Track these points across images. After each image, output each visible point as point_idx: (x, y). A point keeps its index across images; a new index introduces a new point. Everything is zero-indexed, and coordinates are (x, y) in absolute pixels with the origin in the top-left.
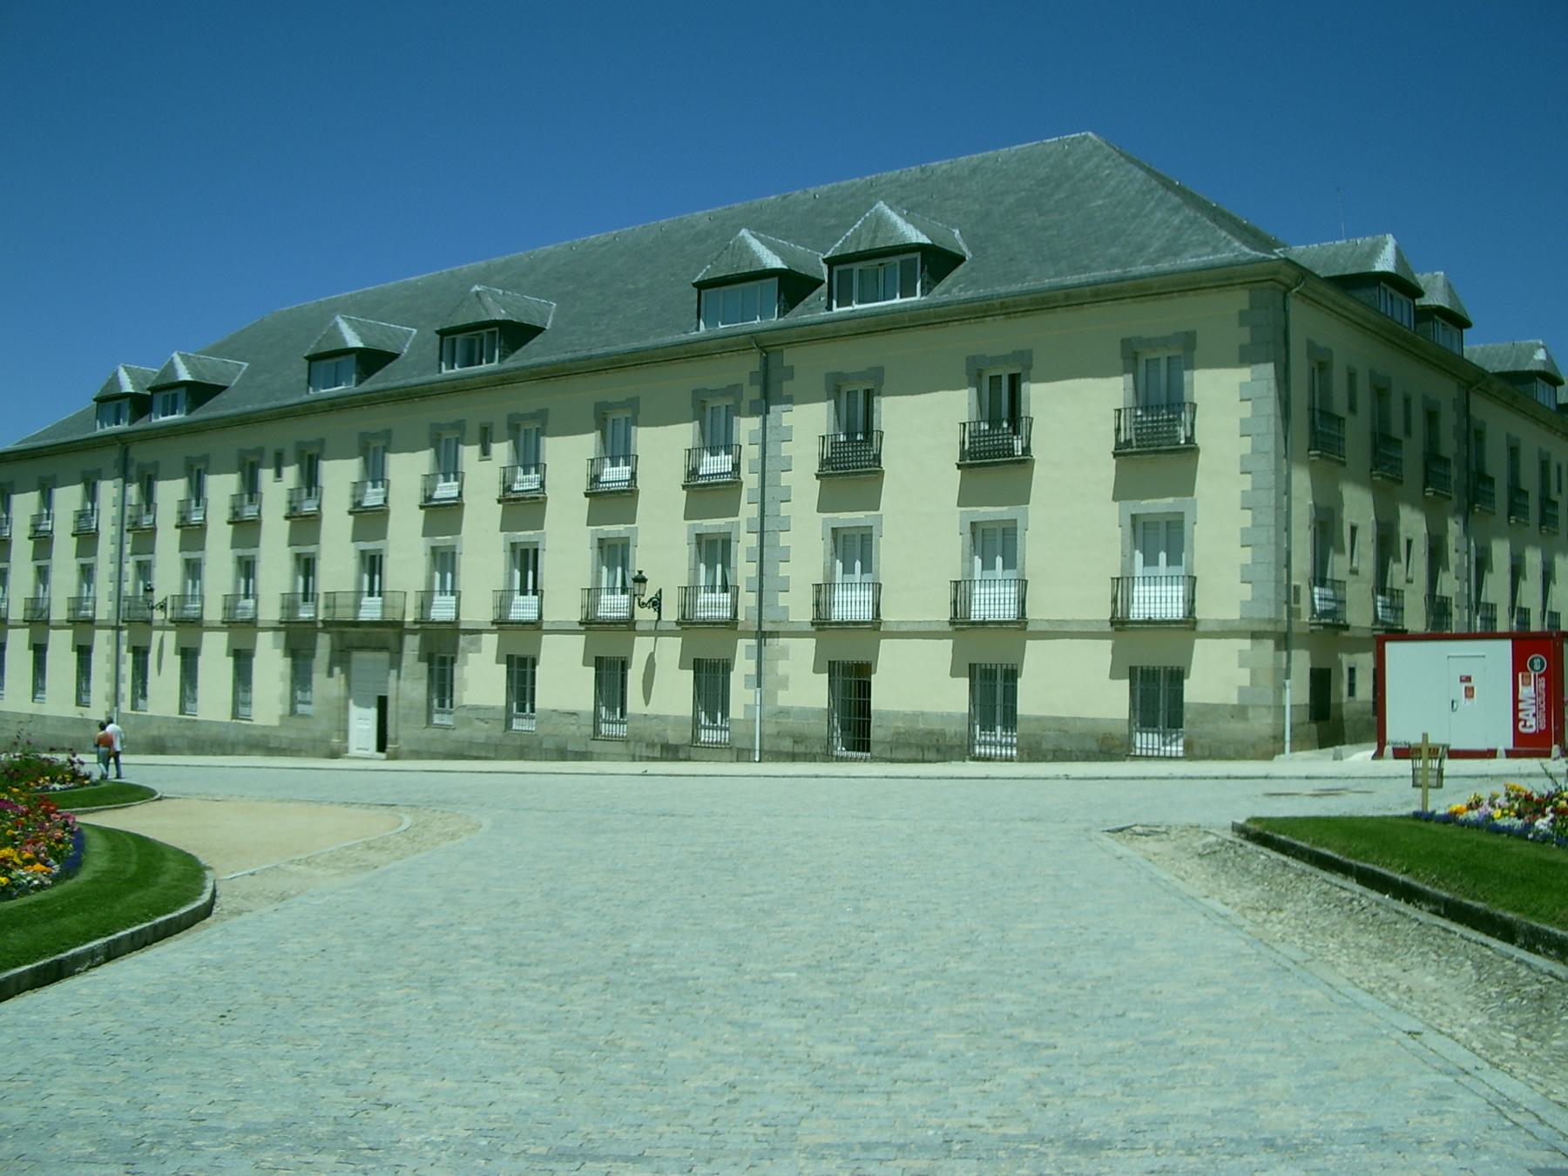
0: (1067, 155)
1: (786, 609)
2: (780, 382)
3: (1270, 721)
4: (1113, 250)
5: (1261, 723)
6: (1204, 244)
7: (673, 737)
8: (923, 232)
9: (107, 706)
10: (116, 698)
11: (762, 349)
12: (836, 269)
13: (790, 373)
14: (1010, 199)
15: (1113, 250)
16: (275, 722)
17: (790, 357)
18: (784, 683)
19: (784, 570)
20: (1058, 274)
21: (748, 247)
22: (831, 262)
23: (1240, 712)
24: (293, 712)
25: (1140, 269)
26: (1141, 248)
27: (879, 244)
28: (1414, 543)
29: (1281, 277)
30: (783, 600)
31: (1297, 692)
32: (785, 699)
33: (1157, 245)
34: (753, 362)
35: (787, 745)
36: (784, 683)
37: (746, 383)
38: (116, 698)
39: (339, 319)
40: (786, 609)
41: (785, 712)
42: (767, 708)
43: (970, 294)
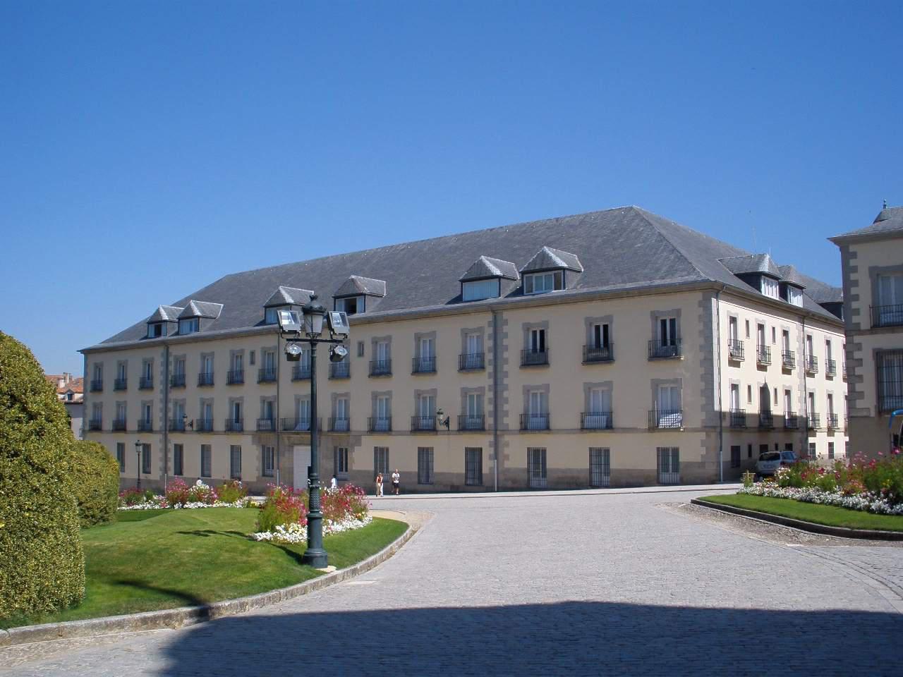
0: (624, 216)
1: (508, 424)
2: (503, 391)
3: (715, 468)
4: (646, 271)
5: (711, 470)
6: (684, 270)
7: (456, 482)
8: (564, 261)
9: (160, 473)
10: (165, 470)
11: (493, 311)
12: (525, 276)
13: (506, 322)
14: (599, 240)
15: (646, 271)
16: (255, 480)
17: (506, 315)
18: (507, 457)
19: (505, 342)
20: (624, 282)
21: (484, 264)
22: (523, 273)
23: (702, 465)
24: (264, 475)
25: (657, 282)
26: (658, 270)
27: (545, 267)
28: (753, 447)
29: (715, 287)
30: (506, 420)
31: (726, 456)
32: (508, 464)
33: (664, 269)
34: (490, 317)
35: (509, 484)
36: (507, 457)
37: (487, 389)
38: (165, 470)
39: (281, 288)
40: (508, 424)
41: (508, 470)
42: (500, 469)
43: (585, 290)
